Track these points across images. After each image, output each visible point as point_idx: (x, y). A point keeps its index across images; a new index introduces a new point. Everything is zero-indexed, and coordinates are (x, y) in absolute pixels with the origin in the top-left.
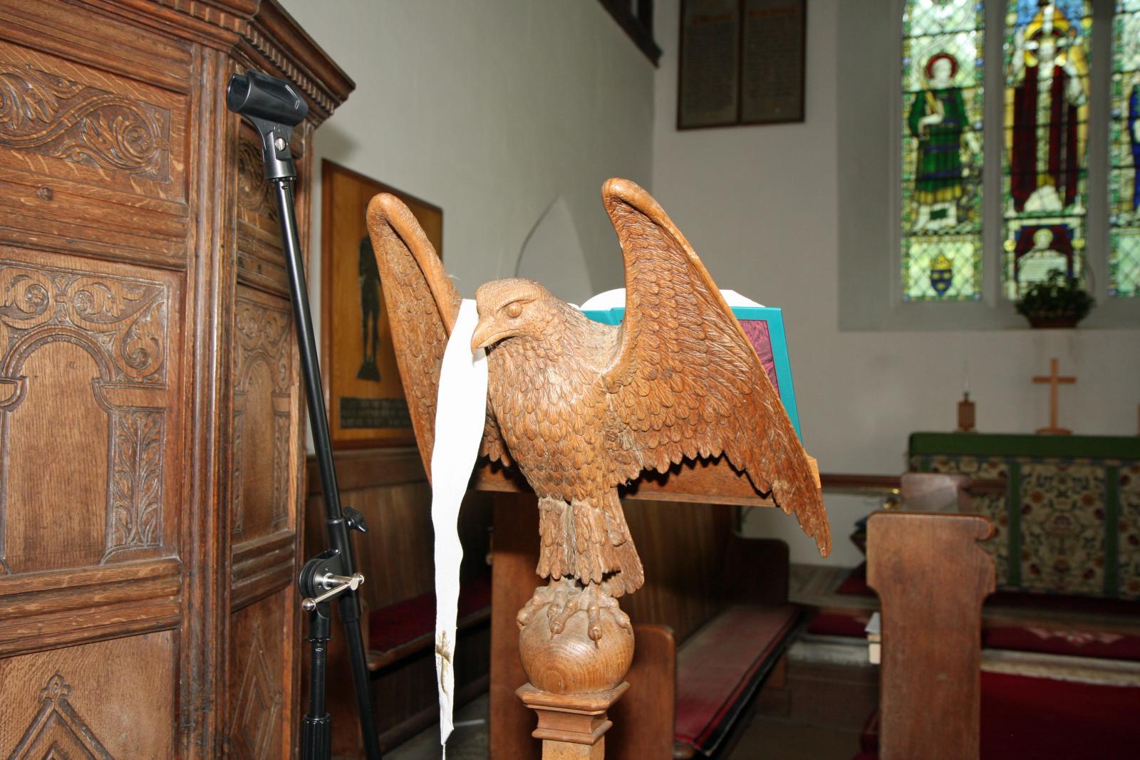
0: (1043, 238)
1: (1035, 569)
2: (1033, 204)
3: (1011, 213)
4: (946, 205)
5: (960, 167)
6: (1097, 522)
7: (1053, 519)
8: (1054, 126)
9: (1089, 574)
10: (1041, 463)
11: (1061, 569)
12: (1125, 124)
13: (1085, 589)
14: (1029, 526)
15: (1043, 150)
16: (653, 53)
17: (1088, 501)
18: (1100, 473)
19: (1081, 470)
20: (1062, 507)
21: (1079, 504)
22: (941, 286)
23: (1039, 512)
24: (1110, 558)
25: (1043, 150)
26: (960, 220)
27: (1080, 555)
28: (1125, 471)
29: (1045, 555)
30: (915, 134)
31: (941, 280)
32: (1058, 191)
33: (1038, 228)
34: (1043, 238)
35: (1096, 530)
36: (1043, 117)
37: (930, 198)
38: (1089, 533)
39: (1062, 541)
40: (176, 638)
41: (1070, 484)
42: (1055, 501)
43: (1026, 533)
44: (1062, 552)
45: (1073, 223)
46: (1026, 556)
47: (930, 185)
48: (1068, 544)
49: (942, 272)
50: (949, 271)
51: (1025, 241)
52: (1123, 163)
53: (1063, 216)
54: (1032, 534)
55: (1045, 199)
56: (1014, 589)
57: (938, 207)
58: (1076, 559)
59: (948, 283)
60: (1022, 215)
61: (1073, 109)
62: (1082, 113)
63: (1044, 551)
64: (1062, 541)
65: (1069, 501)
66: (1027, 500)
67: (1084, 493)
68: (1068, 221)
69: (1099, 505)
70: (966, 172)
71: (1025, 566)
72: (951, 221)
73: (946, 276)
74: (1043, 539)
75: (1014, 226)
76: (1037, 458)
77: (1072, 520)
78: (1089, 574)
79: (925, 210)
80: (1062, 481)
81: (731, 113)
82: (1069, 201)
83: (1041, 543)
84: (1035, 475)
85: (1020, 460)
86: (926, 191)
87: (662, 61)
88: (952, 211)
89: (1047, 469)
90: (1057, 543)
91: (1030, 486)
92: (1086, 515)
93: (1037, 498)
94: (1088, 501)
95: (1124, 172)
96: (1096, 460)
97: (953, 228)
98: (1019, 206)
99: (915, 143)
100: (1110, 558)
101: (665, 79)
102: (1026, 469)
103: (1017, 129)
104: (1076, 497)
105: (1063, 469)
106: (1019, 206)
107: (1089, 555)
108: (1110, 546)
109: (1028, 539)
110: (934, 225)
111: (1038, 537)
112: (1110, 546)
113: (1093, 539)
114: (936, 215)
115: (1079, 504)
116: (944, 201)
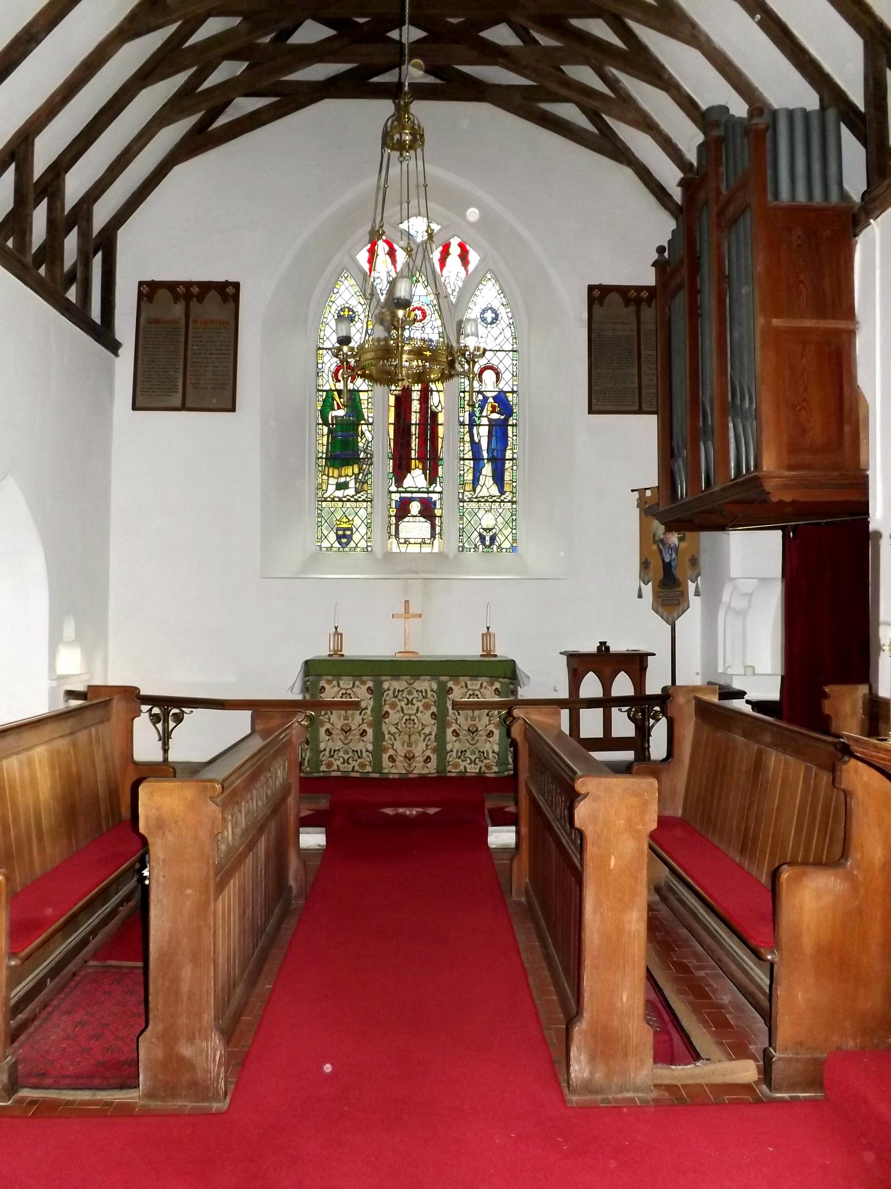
0: (415, 507)
1: (392, 759)
2: (408, 482)
3: (393, 488)
4: (348, 479)
5: (356, 450)
6: (433, 722)
7: (404, 721)
8: (422, 424)
9: (428, 760)
10: (398, 680)
11: (409, 758)
12: (467, 429)
13: (426, 771)
14: (387, 727)
15: (414, 443)
16: (113, 347)
17: (427, 707)
18: (435, 686)
19: (426, 685)
20: (410, 712)
21: (421, 708)
22: (344, 540)
23: (394, 716)
24: (441, 749)
25: (414, 443)
26: (357, 492)
27: (422, 746)
28: (450, 684)
29: (401, 749)
30: (325, 423)
31: (344, 536)
32: (424, 473)
33: (411, 500)
34: (415, 507)
35: (431, 728)
36: (415, 418)
37: (336, 472)
38: (427, 731)
39: (410, 736)
40: (327, 396)
41: (415, 694)
42: (405, 707)
43: (386, 733)
44: (410, 744)
45: (435, 497)
46: (385, 750)
47: (337, 462)
48: (413, 738)
49: (345, 529)
50: (351, 529)
51: (403, 510)
52: (466, 457)
53: (428, 492)
54: (389, 733)
55: (416, 479)
56: (377, 775)
57: (342, 480)
58: (419, 749)
59: (350, 538)
60: (400, 489)
61: (435, 415)
62: (441, 418)
63: (398, 745)
64: (410, 736)
65: (415, 707)
66: (386, 708)
67: (424, 701)
68: (431, 495)
69: (434, 709)
70: (362, 455)
71: (385, 757)
72: (351, 492)
73: (348, 533)
74: (396, 736)
75: (396, 497)
76: (396, 676)
77: (416, 721)
78: (428, 760)
79: (333, 481)
80: (410, 693)
81: (177, 400)
82: (432, 480)
83: (395, 739)
84: (392, 689)
85: (383, 678)
86: (334, 467)
87: (121, 351)
88: (352, 484)
89: (399, 685)
90: (406, 738)
91: (388, 697)
92: (426, 717)
93: (393, 706)
94: (427, 707)
95: (467, 462)
96: (434, 676)
97: (352, 497)
98: (399, 483)
99: (326, 429)
100: (441, 749)
101: (124, 365)
102: (386, 685)
103: (397, 425)
104: (420, 704)
105: (410, 684)
106: (399, 483)
107: (427, 746)
108: (441, 738)
109: (387, 737)
110: (339, 493)
111: (393, 735)
112: (441, 738)
113: (430, 734)
114: (341, 486)
115: (421, 708)
116: (346, 476)
